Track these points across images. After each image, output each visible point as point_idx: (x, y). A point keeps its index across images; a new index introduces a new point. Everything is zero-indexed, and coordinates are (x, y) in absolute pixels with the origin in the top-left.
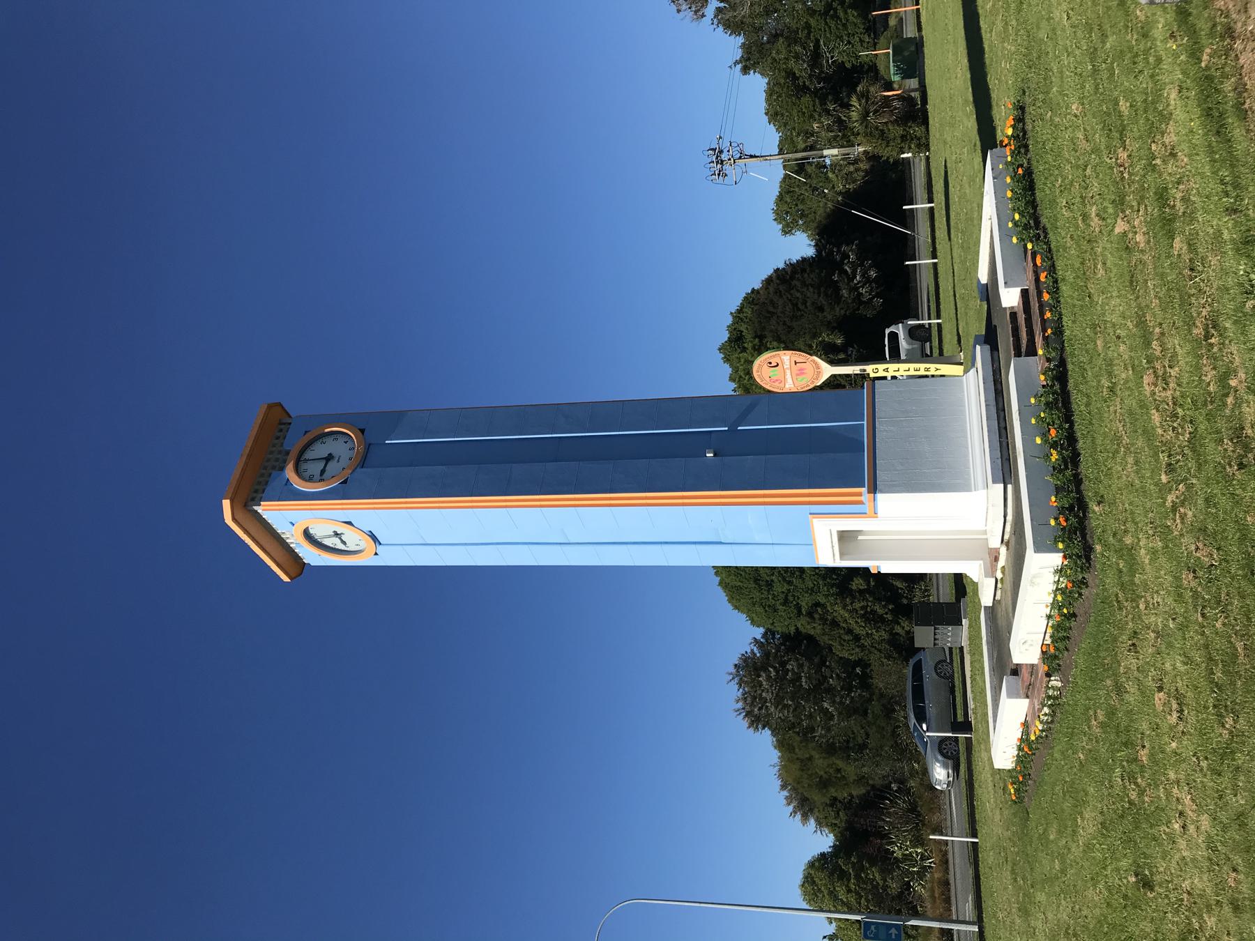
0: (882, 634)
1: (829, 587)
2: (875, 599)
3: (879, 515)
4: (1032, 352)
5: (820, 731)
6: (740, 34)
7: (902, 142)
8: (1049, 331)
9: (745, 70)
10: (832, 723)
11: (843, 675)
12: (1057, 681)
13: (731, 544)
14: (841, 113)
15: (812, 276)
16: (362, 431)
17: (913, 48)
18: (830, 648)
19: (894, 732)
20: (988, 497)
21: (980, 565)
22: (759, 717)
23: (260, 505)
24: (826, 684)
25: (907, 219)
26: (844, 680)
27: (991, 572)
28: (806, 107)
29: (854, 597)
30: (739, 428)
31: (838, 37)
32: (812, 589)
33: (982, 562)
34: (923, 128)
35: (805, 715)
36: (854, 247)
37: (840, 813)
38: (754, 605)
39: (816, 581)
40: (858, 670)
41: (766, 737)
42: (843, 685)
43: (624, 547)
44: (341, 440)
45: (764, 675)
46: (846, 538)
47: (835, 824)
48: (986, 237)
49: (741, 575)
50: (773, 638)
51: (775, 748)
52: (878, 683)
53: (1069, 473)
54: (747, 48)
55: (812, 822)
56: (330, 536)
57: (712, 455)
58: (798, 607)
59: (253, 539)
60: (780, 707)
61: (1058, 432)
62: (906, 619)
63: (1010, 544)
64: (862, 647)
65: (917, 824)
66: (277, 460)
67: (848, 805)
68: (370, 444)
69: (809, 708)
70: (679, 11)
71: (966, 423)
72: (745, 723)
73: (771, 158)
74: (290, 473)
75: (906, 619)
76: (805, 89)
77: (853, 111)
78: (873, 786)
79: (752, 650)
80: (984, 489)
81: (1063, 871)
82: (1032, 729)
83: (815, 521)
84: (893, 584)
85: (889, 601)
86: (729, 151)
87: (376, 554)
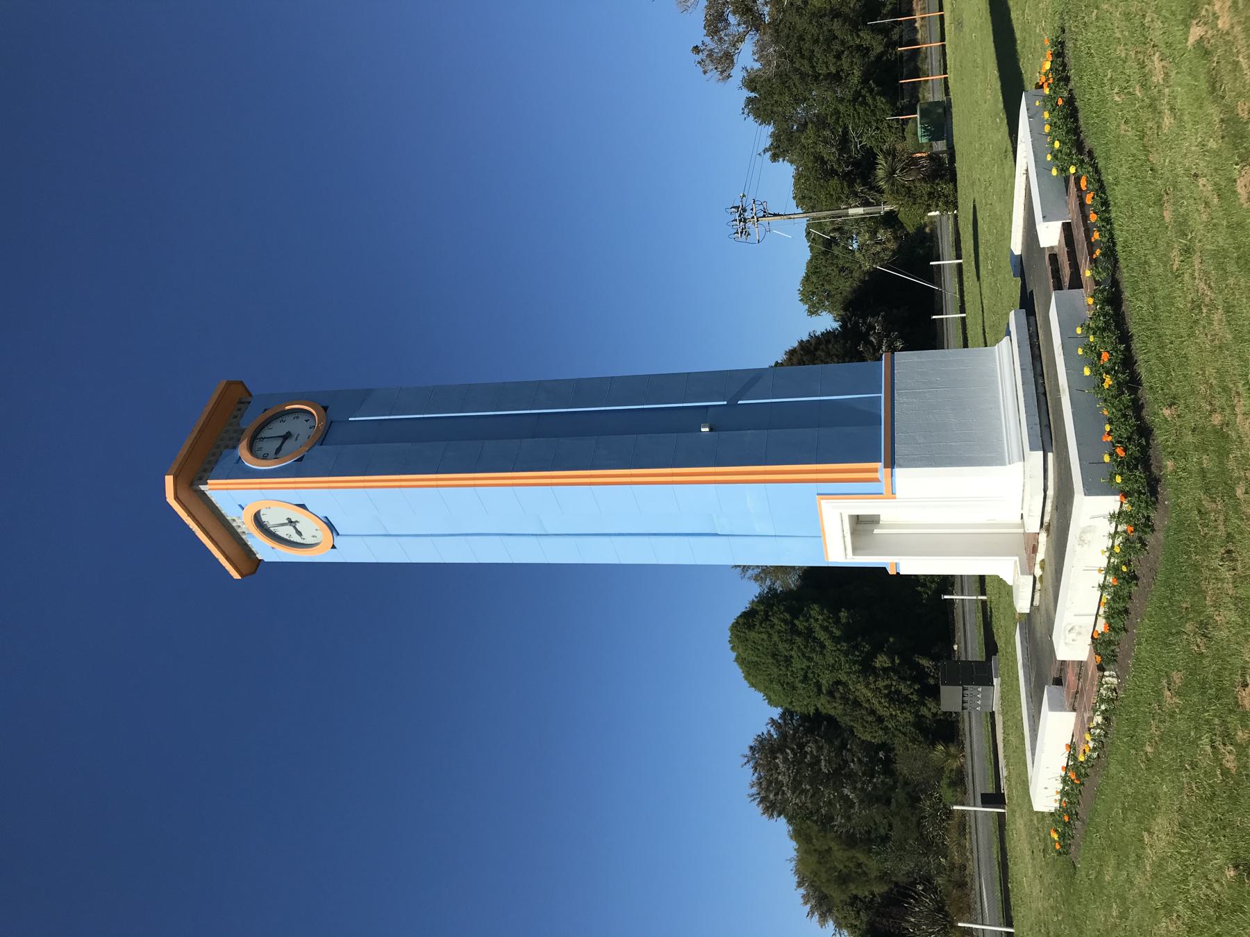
0: (908, 716)
1: (852, 664)
2: (900, 678)
3: (897, 496)
4: (1076, 283)
5: (839, 820)
6: (770, 124)
7: (929, 199)
8: (1098, 252)
9: (775, 158)
10: (852, 811)
11: (865, 759)
12: (1113, 677)
13: (728, 535)
14: (869, 195)
15: (836, 346)
16: (325, 409)
17: (940, 110)
18: (851, 730)
19: (919, 823)
20: (1024, 471)
21: (1016, 562)
22: (774, 803)
23: (207, 484)
24: (847, 769)
25: (934, 275)
26: (866, 764)
27: (1028, 568)
28: (834, 189)
29: (877, 676)
30: (739, 402)
31: (866, 122)
32: (833, 666)
33: (1017, 558)
34: (951, 186)
35: (824, 802)
36: (880, 318)
37: (861, 913)
38: (772, 682)
39: (838, 657)
40: (881, 755)
41: (781, 826)
42: (865, 770)
43: (607, 539)
44: (303, 418)
45: (781, 757)
46: (861, 525)
47: (856, 926)
48: (1020, 182)
49: (759, 650)
50: (792, 719)
51: (791, 837)
52: (902, 767)
53: (1126, 397)
54: (777, 137)
55: (831, 924)
56: (283, 525)
57: (707, 430)
58: (819, 686)
59: (190, 514)
60: (798, 792)
61: (1112, 355)
62: (933, 701)
63: (1051, 527)
64: (886, 729)
65: (945, 925)
66: (231, 439)
67: (869, 905)
68: (332, 422)
69: (828, 793)
70: (705, 72)
71: (998, 393)
72: (760, 809)
73: (795, 216)
74: (243, 451)
75: (933, 701)
76: (833, 172)
77: (880, 169)
78: (896, 884)
79: (769, 731)
80: (1020, 461)
81: (1123, 916)
82: (1082, 747)
83: (823, 502)
84: (919, 663)
85: (915, 680)
86: (752, 209)
87: (333, 547)
